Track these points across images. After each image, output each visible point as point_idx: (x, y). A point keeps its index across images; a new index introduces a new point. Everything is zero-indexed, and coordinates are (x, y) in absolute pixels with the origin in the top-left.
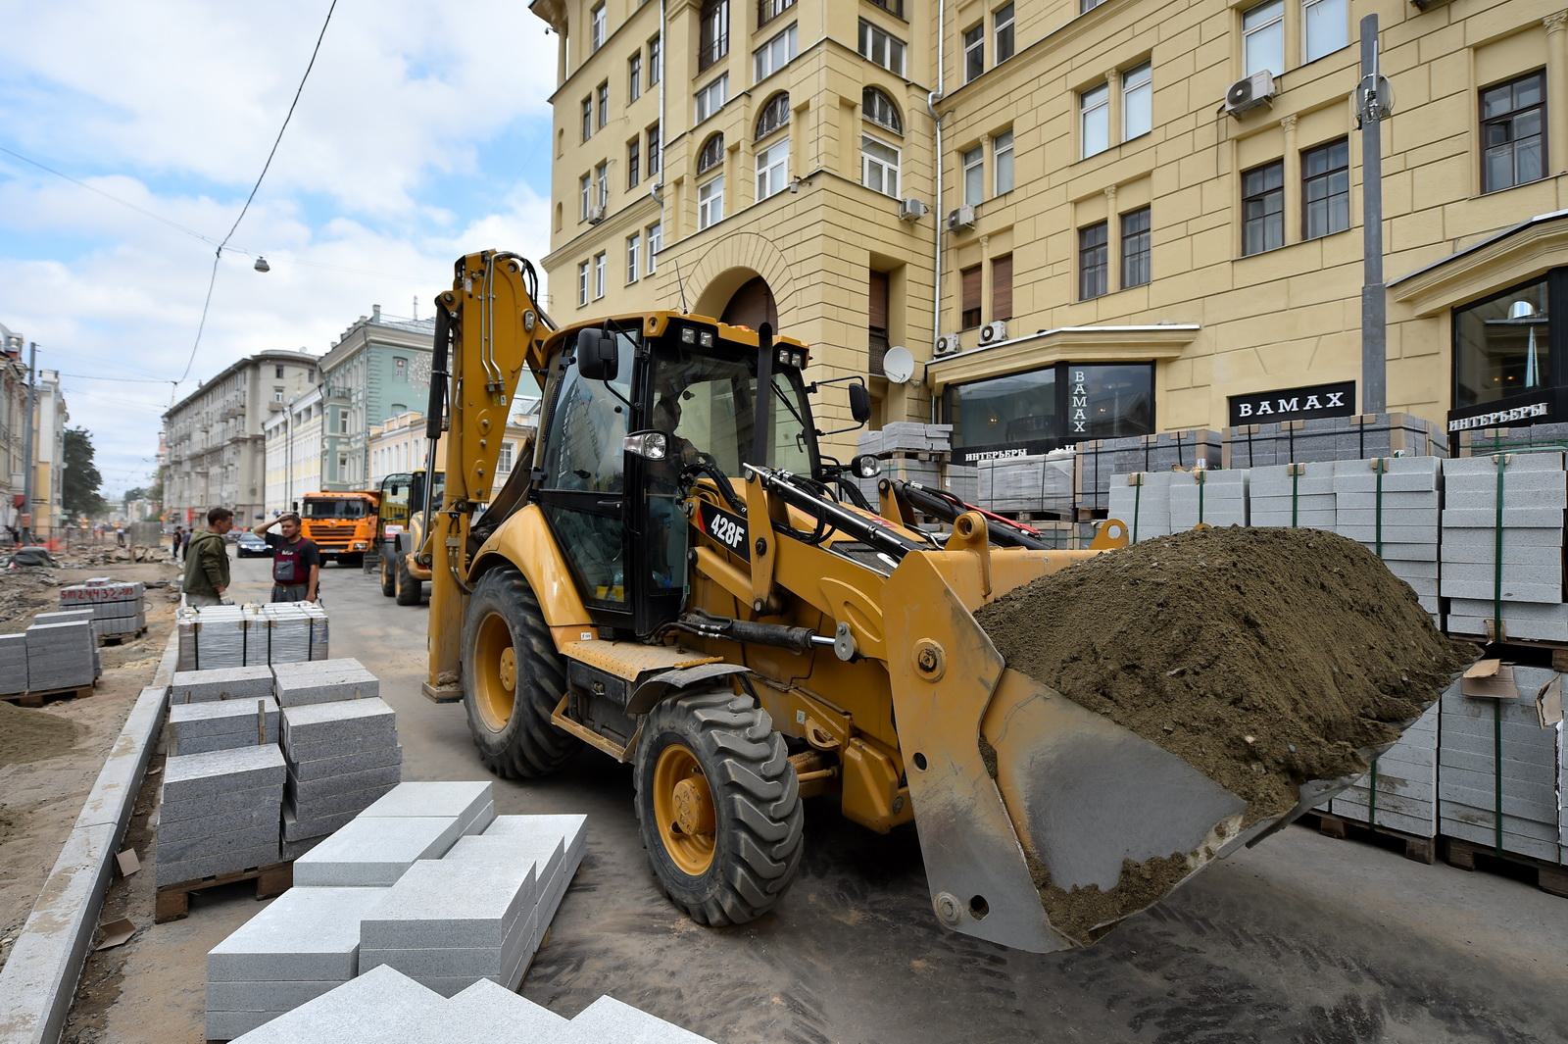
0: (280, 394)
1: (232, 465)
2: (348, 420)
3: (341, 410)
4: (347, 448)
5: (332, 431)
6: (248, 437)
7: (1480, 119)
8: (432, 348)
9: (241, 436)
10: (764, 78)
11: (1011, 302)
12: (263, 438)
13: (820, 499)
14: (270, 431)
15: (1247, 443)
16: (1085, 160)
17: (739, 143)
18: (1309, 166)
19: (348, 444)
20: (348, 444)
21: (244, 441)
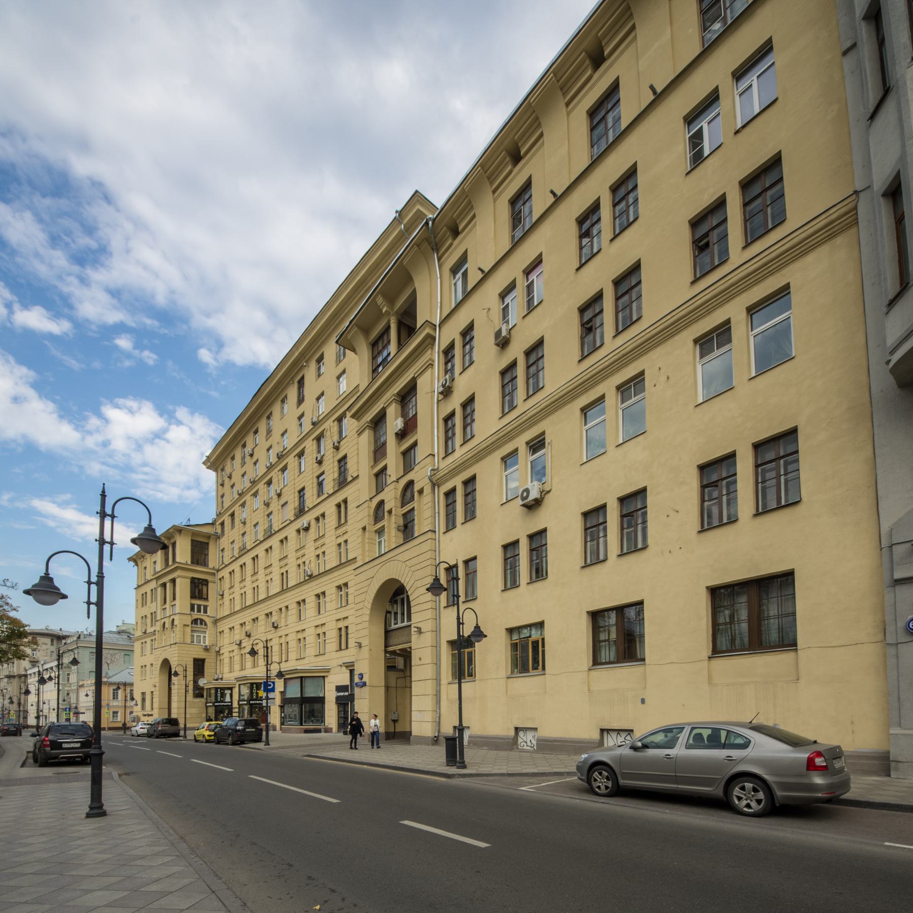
0: (35, 652)
1: (6, 689)
2: (70, 677)
3: (67, 672)
4: (70, 689)
5: (63, 681)
6: (16, 674)
7: (621, 513)
8: (95, 646)
9: (11, 674)
10: (634, 320)
11: (794, 594)
12: (26, 676)
13: (225, 702)
14: (31, 674)
15: (269, 701)
16: (319, 574)
17: (391, 509)
18: (875, 762)
19: (70, 687)
20: (70, 687)
21: (14, 677)
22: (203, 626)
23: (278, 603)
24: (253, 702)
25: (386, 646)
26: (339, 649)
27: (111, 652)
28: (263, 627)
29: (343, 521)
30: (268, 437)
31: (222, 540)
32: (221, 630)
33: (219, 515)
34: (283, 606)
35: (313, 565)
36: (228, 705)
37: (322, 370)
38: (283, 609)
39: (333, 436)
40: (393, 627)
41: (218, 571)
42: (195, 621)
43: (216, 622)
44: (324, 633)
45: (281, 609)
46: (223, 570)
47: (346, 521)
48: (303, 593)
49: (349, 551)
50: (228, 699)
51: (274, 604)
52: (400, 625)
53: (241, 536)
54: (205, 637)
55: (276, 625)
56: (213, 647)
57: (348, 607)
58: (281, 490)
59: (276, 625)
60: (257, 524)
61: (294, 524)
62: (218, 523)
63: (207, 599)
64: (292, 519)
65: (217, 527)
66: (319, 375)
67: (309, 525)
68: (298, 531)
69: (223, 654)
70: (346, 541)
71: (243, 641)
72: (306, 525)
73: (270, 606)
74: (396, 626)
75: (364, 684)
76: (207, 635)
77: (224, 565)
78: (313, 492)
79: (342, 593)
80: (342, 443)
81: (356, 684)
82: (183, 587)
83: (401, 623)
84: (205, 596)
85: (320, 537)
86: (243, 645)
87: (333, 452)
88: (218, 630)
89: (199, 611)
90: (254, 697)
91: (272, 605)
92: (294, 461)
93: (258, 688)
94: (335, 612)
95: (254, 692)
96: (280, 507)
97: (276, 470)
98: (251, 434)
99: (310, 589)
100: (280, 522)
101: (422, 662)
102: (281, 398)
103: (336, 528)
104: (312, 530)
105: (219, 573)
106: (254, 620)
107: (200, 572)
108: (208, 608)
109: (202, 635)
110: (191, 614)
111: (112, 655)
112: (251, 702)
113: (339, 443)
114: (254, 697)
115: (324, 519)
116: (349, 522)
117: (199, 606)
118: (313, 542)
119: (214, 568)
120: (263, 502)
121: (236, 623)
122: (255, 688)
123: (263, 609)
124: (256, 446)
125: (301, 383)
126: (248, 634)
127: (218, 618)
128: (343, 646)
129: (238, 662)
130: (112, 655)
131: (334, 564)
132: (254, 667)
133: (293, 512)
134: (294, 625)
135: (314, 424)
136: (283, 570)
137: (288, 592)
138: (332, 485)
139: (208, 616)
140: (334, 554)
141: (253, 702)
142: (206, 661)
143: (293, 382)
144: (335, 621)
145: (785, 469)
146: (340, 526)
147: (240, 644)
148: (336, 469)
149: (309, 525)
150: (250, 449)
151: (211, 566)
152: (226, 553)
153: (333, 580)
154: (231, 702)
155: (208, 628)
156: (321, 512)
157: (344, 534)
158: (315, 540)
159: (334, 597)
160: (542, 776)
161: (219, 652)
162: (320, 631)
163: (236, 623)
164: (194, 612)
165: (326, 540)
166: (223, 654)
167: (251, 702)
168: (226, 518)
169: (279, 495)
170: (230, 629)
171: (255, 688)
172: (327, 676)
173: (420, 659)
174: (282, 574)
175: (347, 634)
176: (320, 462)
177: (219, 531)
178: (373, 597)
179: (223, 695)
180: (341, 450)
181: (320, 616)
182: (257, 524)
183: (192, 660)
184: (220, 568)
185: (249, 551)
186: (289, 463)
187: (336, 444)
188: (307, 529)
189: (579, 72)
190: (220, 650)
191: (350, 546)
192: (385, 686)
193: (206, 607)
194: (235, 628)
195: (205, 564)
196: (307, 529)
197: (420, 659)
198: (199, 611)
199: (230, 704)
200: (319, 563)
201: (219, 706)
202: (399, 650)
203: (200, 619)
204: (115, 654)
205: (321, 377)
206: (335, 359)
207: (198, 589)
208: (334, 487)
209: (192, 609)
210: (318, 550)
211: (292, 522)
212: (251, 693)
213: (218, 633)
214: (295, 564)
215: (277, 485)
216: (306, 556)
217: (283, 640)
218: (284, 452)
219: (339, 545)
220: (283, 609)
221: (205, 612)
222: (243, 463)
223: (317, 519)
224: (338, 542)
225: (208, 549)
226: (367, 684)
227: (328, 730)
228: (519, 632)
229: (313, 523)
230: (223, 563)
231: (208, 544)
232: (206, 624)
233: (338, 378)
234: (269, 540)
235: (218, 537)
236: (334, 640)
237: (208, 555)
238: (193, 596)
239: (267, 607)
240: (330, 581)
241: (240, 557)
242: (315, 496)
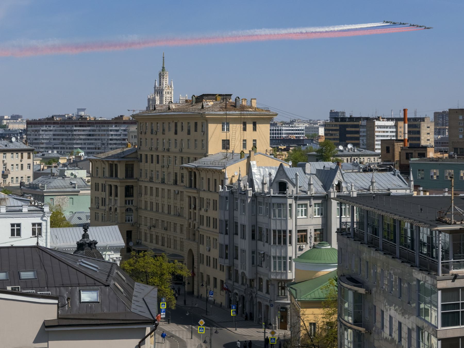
27: (62, 197)
42: (127, 210)
54: (132, 218)
76: (133, 217)
82: (121, 191)
89: (129, 204)
107: (130, 182)
108: (133, 201)
109: (130, 217)
110: (125, 206)
111: (62, 199)
117: (129, 201)
119: (136, 178)
130: (62, 199)
142: (133, 232)
145: (391, 240)
151: (135, 177)
164: (126, 204)
178: (187, 255)
183: (126, 232)
189: (128, 322)
193: (132, 201)
198: (129, 204)
204: (64, 198)
207: (129, 191)
209: (126, 203)
221: (132, 204)
228: (277, 274)
232: (132, 211)
238: (126, 196)
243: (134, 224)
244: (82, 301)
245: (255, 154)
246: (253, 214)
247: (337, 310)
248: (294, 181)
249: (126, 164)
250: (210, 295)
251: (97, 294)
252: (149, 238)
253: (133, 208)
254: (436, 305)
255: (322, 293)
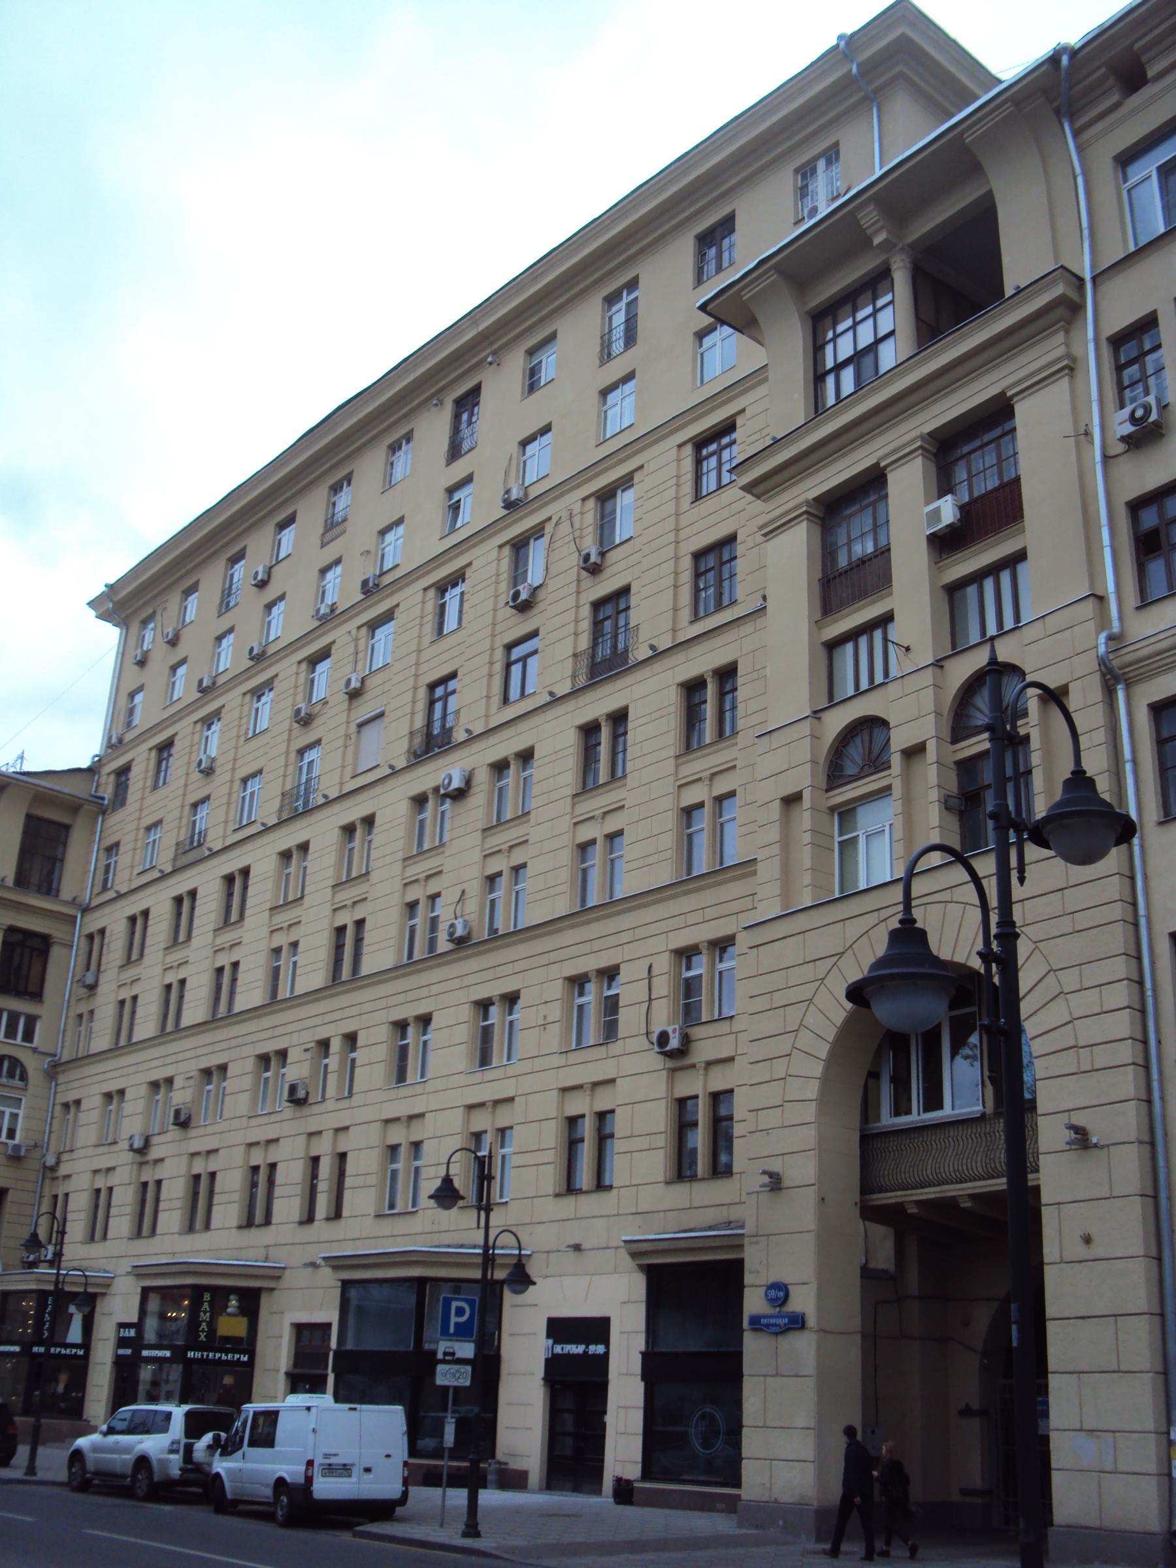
22: (16, 1082)
23: (318, 1020)
24: (198, 1355)
25: (866, 1188)
26: (333, 1215)
28: (245, 1098)
29: (234, 917)
30: (328, 536)
31: (114, 819)
32: (71, 1097)
33: (114, 745)
34: (334, 1032)
35: (472, 906)
36: (75, 1356)
37: (398, 473)
38: (336, 1045)
39: (581, 537)
40: (887, 1120)
41: (86, 910)
43: (55, 1069)
44: (417, 1146)
45: (324, 1044)
46: (107, 910)
47: (142, 955)
48: (424, 992)
49: (298, 972)
50: (75, 1334)
51: (298, 1026)
52: (916, 1116)
53: (142, 831)
54: (14, 1116)
55: (301, 1094)
56: (37, 1154)
57: (616, 1048)
58: (363, 681)
59: (301, 1094)
60: (157, 824)
61: (403, 779)
62: (107, 769)
63: (37, 995)
64: (563, 688)
65: (103, 780)
66: (532, 387)
67: (468, 782)
68: (420, 801)
69: (68, 1177)
70: (518, 869)
71: (155, 1140)
72: (456, 783)
73: (278, 1031)
74: (904, 1120)
75: (797, 1323)
76: (21, 1113)
77: (111, 894)
78: (227, 813)
79: (268, 1074)
80: (613, 556)
81: (755, 1321)
83: (927, 1109)
84: (32, 988)
85: (286, 904)
86: (155, 1153)
87: (290, 730)
88: (61, 1098)
90: (203, 1337)
91: (289, 1028)
92: (297, 674)
93: (219, 1307)
94: (557, 1060)
95: (205, 1317)
96: (353, 728)
97: (352, 625)
98: (270, 527)
99: (456, 983)
100: (232, 827)
101: (1097, 1250)
102: (331, 482)
103: (166, 949)
104: (478, 798)
105: (88, 918)
106: (207, 1073)
109: (8, 1111)
112: (191, 1354)
113: (602, 554)
114: (203, 1337)
115: (370, 833)
116: (248, 921)
118: (479, 834)
119: (73, 902)
120: (289, 713)
121: (183, 1067)
122: (206, 1306)
123: (289, 1028)
124: (278, 562)
125: (469, 401)
126: (182, 1118)
127: (65, 1058)
128: (585, 1177)
129: (128, 1209)
131: (562, 906)
132: (92, 1239)
133: (404, 745)
134: (91, 1151)
135: (511, 505)
136: (224, 960)
137: (230, 1025)
138: (172, 855)
139: (35, 1050)
140: (393, 931)
141: (198, 1355)
143: (441, 403)
144: (555, 1093)
146: (226, 923)
147: (143, 1150)
148: (586, 625)
149: (468, 782)
150: (260, 569)
151: (66, 892)
152: (124, 859)
153: (554, 956)
154: (86, 1344)
155: (31, 1088)
156: (189, 886)
157: (180, 965)
158: (484, 830)
159: (555, 1012)
160: (389, 1542)
161: (53, 1169)
162: (397, 1135)
163: (183, 1067)
165: (534, 831)
166: (68, 1177)
167: (191, 1354)
168: (142, 759)
169: (354, 695)
170: (108, 1096)
171: (206, 1306)
172: (272, 1290)
173: (1087, 1240)
174: (341, 930)
175: (157, 1200)
176: (305, 721)
177: (107, 792)
179: (61, 1320)
180: (607, 573)
181: (403, 1092)
182: (157, 824)
184: (94, 904)
185: (214, 854)
186: (280, 677)
187: (593, 558)
188: (460, 795)
190: (58, 1163)
191: (528, 883)
192: (864, 1336)
193: (31, 1021)
194: (129, 1095)
195: (49, 887)
196: (460, 795)
197: (1087, 1240)
199: (81, 1352)
200: (493, 902)
201: (201, 1361)
202: (918, 1203)
203: (10, 1058)
205: (536, 395)
206: (598, 349)
208: (574, 677)
210: (276, 935)
211: (395, 773)
212: (194, 1322)
213: (58, 1108)
214: (566, 840)
215: (350, 667)
216: (444, 876)
217: (324, 1148)
218: (388, 579)
219: (412, 906)
220: (336, 1045)
221: (28, 1036)
222: (225, 606)
223: (500, 767)
224: (410, 898)
225: (65, 844)
226: (811, 1321)
227: (513, 1480)
229: (482, 777)
230: (105, 888)
231: (67, 828)
232: (24, 1077)
233: (219, 639)
234: (299, 824)
235: (103, 810)
236: (550, 1156)
237: (62, 860)
239: (268, 1034)
240: (544, 959)
241: (175, 871)
242: (686, 614)
243: (23, 1153)
244: (272, 1500)
245: (350, 704)
246: (317, 1470)
247: (491, 1252)
248: (459, 524)
249: (29, 817)
250: (445, 1331)
251: (267, 1497)
252: (83, 1215)
253: (32, 1064)
254: (850, 769)
255: (312, 1435)
